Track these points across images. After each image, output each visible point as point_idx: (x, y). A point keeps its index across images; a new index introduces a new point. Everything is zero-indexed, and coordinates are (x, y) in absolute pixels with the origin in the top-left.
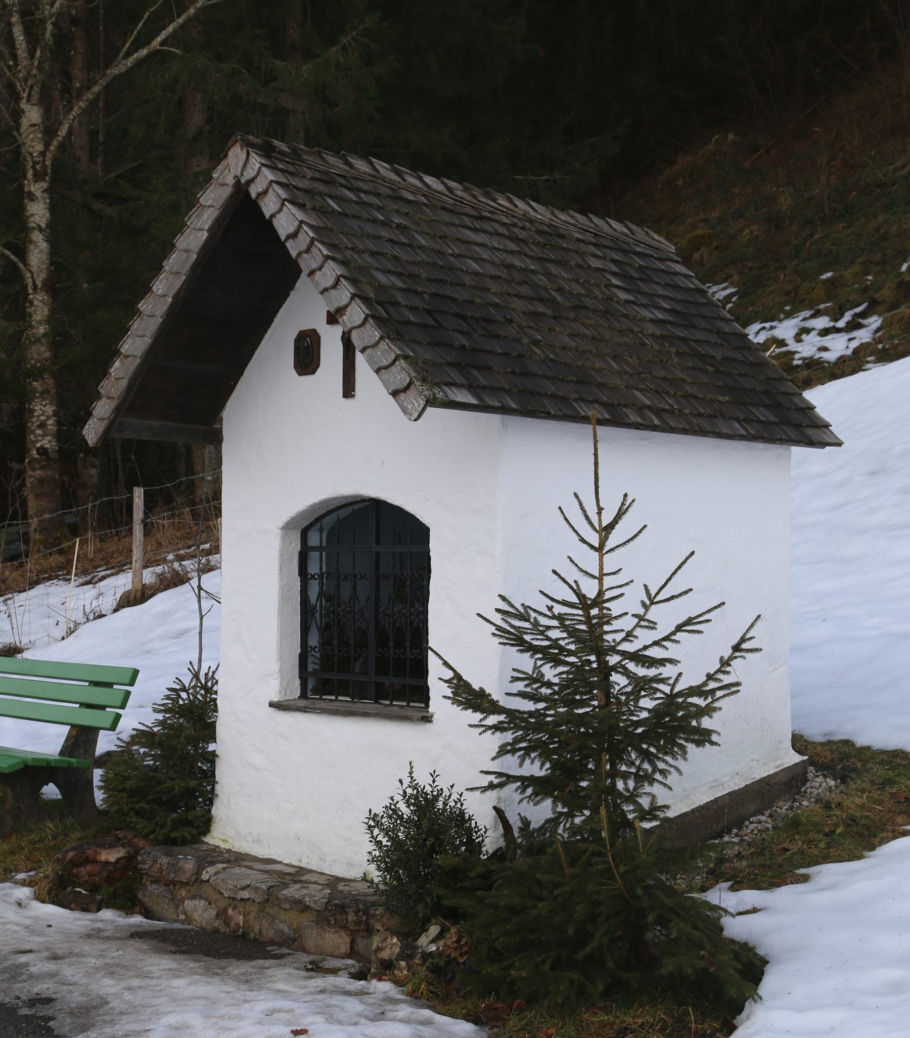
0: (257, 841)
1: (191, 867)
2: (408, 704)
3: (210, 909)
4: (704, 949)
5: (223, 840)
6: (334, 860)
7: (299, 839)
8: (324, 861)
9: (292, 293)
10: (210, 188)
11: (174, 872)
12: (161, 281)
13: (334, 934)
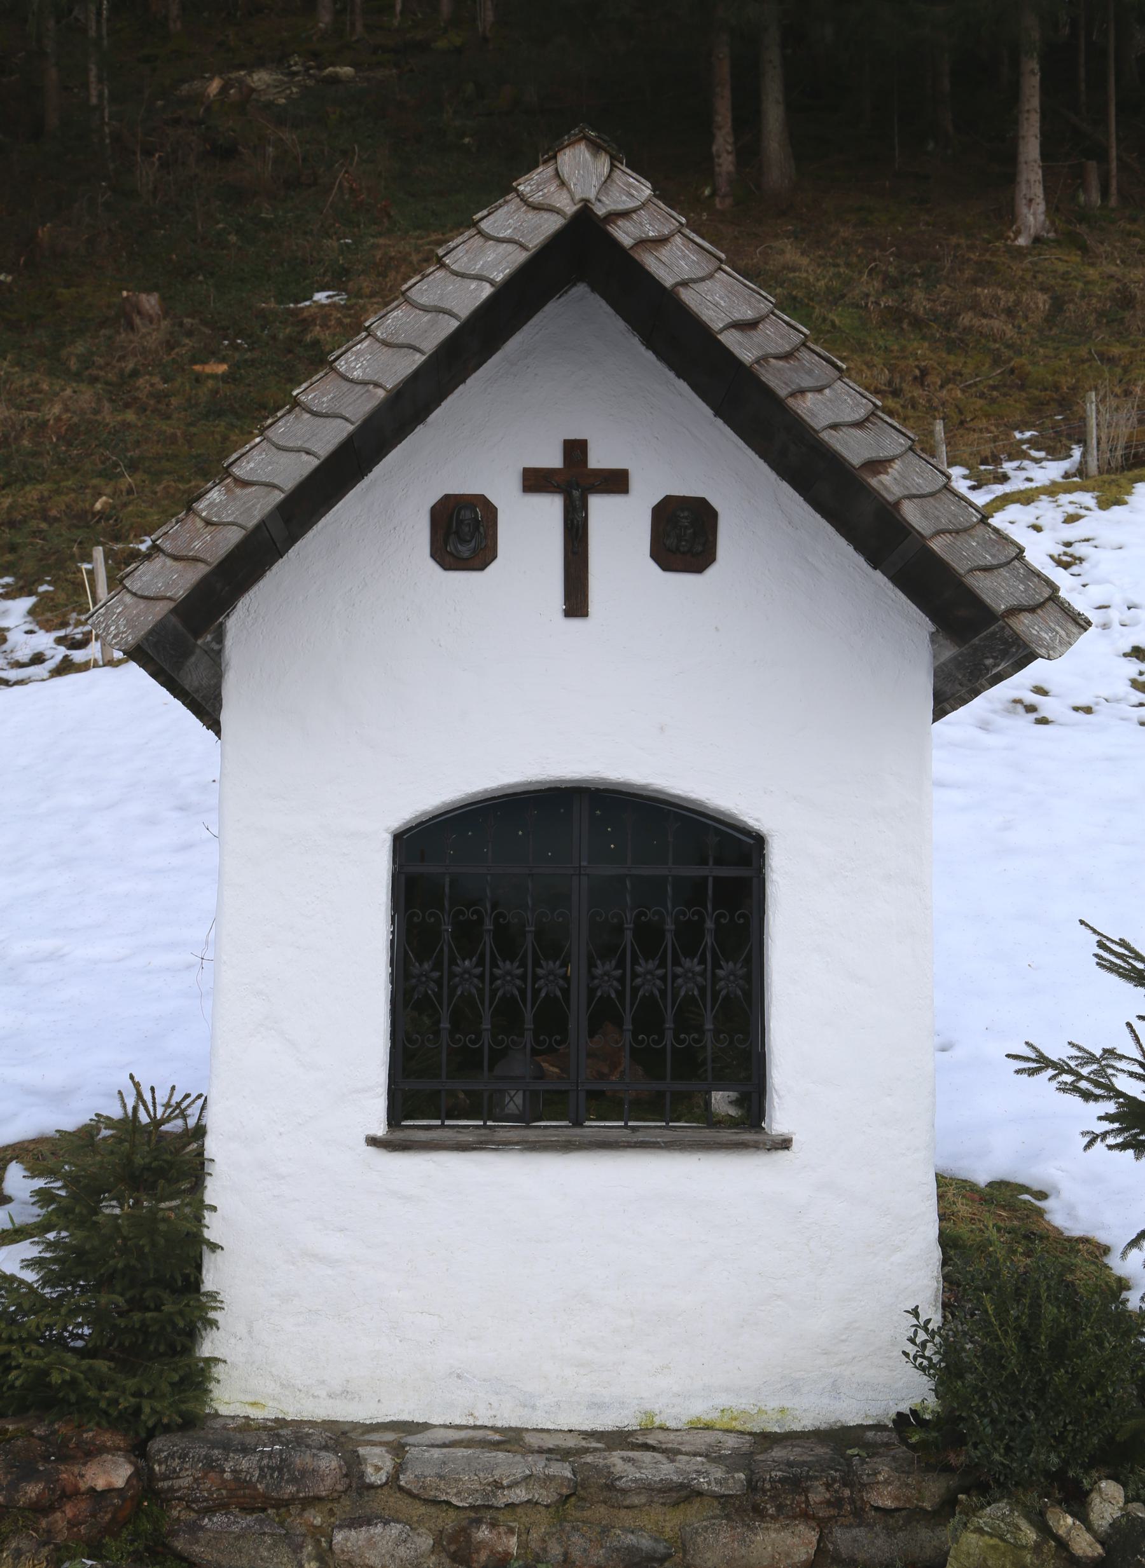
0: (345, 1393)
1: (334, 1464)
2: (485, 1123)
3: (416, 1539)
4: (40, 1438)
5: (254, 1404)
6: (558, 1404)
7: (459, 1377)
8: (534, 1407)
9: (420, 428)
10: (505, 209)
11: (293, 1480)
12: (358, 354)
13: (777, 1531)
